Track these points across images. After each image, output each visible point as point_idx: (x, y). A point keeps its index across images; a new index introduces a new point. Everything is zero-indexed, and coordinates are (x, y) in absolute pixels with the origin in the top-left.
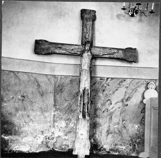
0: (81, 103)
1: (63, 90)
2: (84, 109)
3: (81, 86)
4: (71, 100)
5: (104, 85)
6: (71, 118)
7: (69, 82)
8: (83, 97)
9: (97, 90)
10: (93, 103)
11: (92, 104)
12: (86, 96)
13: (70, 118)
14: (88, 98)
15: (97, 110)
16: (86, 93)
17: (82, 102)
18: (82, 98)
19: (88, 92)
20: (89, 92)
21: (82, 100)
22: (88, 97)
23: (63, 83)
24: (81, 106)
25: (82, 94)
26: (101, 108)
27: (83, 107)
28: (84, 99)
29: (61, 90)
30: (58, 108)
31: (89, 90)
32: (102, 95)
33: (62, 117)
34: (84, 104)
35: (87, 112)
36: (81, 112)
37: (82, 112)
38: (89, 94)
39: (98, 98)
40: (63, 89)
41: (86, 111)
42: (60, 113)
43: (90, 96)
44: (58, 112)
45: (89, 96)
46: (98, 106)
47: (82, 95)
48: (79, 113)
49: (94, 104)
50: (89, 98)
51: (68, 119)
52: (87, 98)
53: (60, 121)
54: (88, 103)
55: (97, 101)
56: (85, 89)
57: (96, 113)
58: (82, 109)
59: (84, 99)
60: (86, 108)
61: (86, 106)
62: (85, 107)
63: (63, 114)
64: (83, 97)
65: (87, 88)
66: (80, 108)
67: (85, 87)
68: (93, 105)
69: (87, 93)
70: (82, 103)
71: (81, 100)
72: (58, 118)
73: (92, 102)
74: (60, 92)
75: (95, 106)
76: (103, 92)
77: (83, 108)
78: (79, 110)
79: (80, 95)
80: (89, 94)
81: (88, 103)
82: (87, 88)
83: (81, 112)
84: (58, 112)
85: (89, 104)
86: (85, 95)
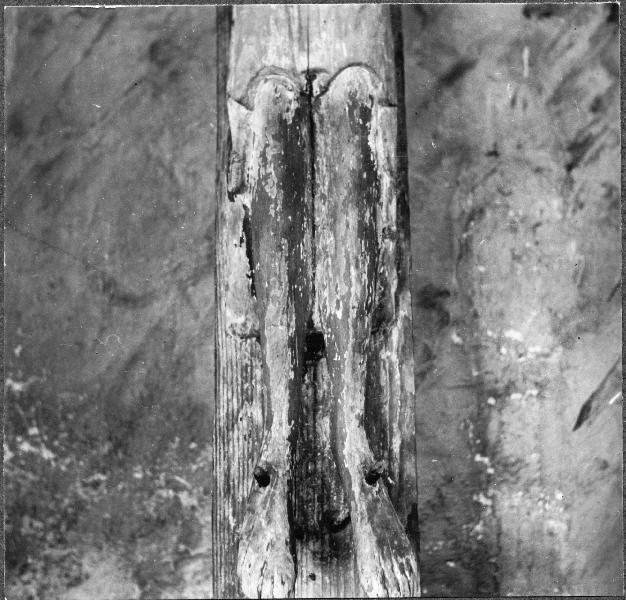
0: (258, 336)
1: (72, 170)
2: (325, 424)
3: (249, 51)
4: (183, 290)
5: (582, 81)
6: (185, 499)
7: (143, 68)
8: (293, 234)
9: (494, 153)
10: (453, 308)
11: (445, 321)
12: (333, 215)
13: (177, 502)
14: (373, 249)
15: (510, 387)
16: (335, 159)
17: (272, 309)
18: (265, 250)
19: (366, 150)
20: (381, 146)
21: (278, 292)
22: (367, 233)
23: (66, 86)
24: (265, 380)
25: (273, 191)
26: (548, 374)
27: (295, 387)
28: (297, 274)
29: (44, 170)
30: (27, 399)
31: (381, 116)
32: (556, 203)
33: (79, 505)
34: (310, 347)
35: (371, 477)
36: (263, 479)
37: (283, 471)
38: (386, 181)
39: (506, 254)
40: (60, 158)
41: (354, 449)
42: (47, 454)
43: (404, 209)
44: (26, 447)
45: (388, 212)
46: (517, 345)
47: (262, 199)
48: (242, 493)
49: (457, 323)
50: (390, 246)
51: (162, 523)
52: (352, 244)
53: (57, 553)
54: (380, 320)
55: (501, 286)
56: (307, 98)
57: (492, 437)
58: (281, 430)
59: (297, 274)
60: (351, 404)
61: (347, 376)
62: (337, 381)
63: (95, 466)
64: (293, 234)
65: (337, 93)
66: (256, 412)
67: (302, 64)
68: (457, 339)
69: (351, 160)
70: (279, 330)
71: (253, 290)
72: (35, 513)
73: (430, 300)
74: (34, 202)
75: (472, 352)
76: (570, 167)
77: (304, 411)
78: (238, 447)
79: (246, 199)
80: (386, 181)
81: (380, 320)
82: (337, 93)
83: (263, 479)
84: (26, 447)
85: (396, 334)
86: (322, 209)
